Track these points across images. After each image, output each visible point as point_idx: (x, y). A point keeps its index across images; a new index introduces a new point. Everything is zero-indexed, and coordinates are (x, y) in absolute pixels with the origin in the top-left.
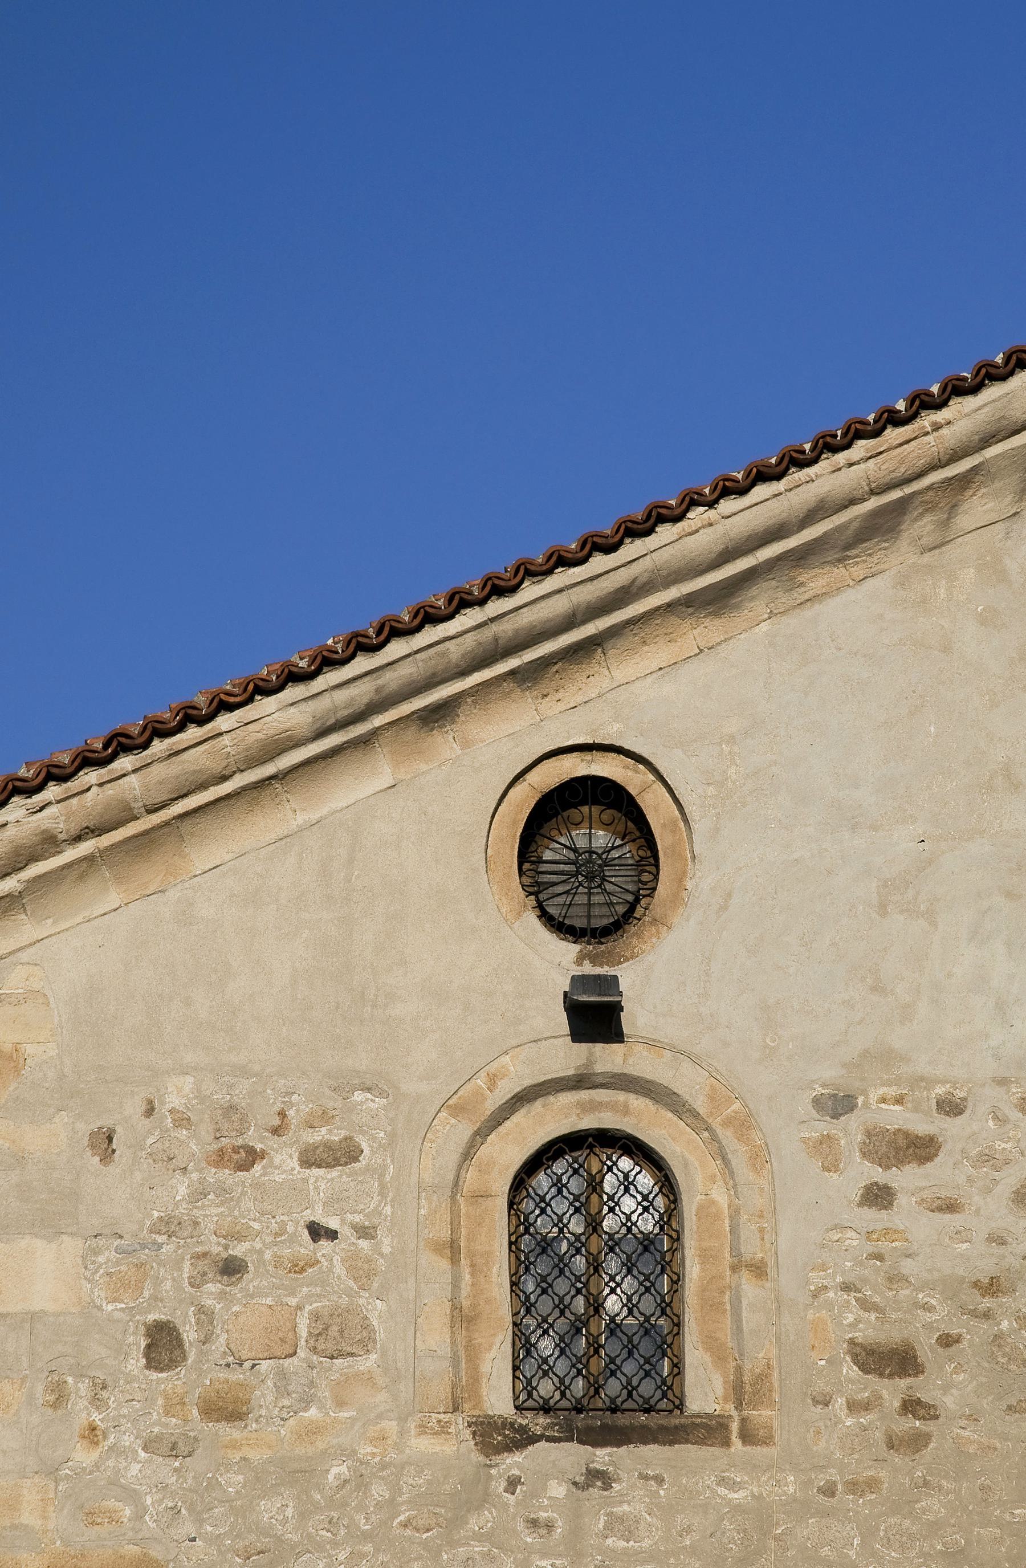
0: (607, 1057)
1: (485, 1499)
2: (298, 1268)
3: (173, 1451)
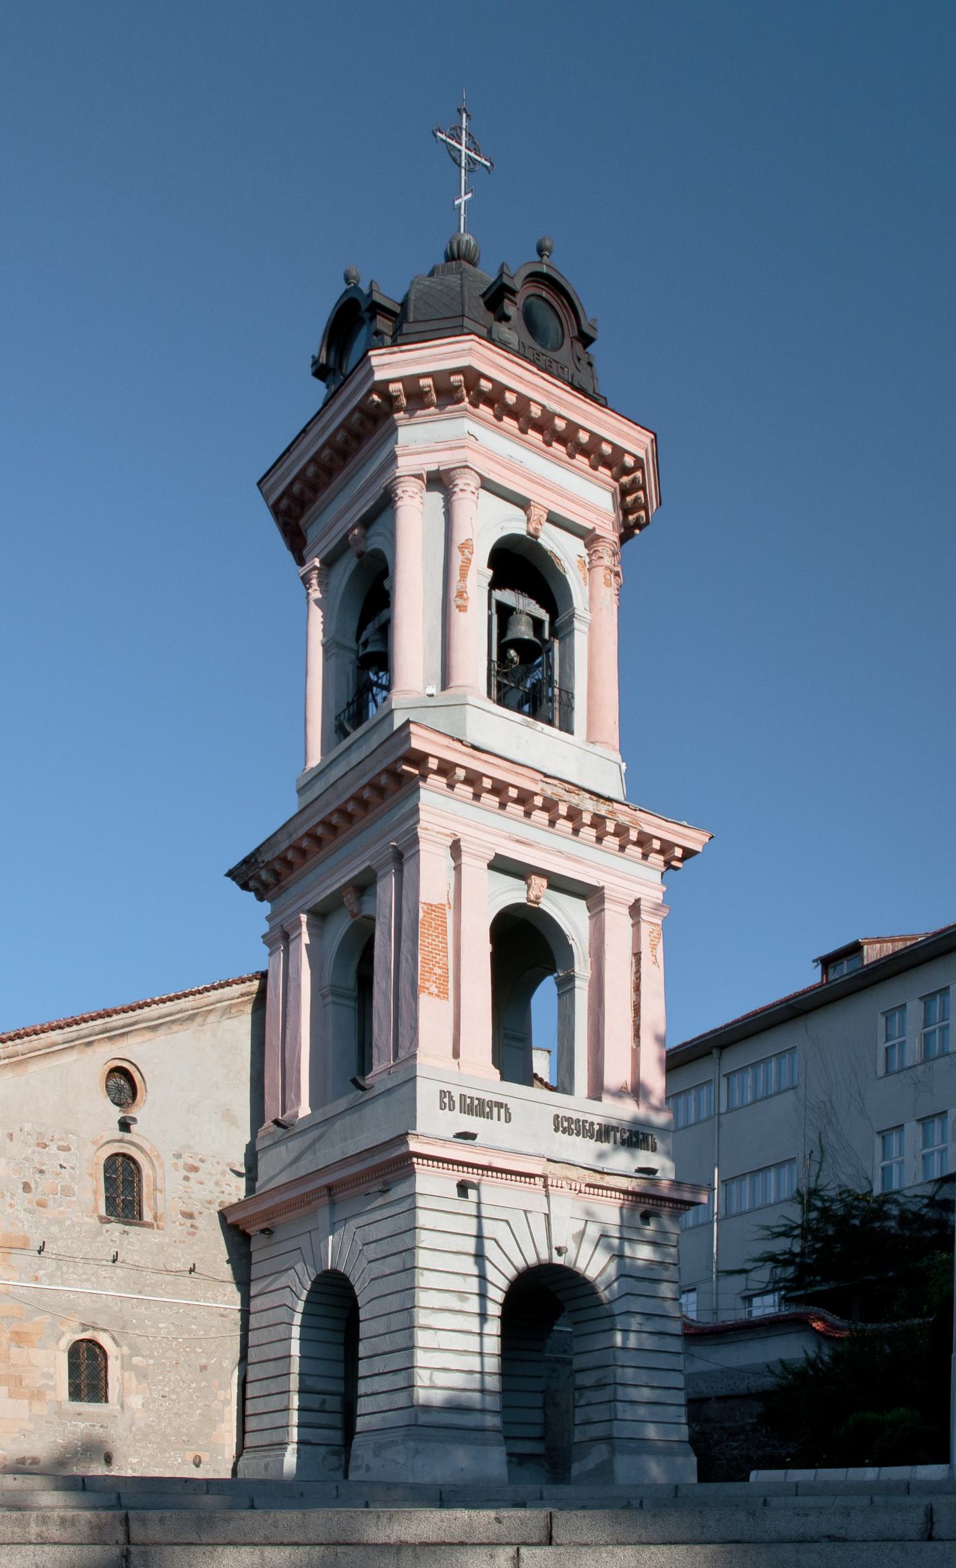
0: (127, 1136)
1: (101, 1234)
3: (30, 1212)
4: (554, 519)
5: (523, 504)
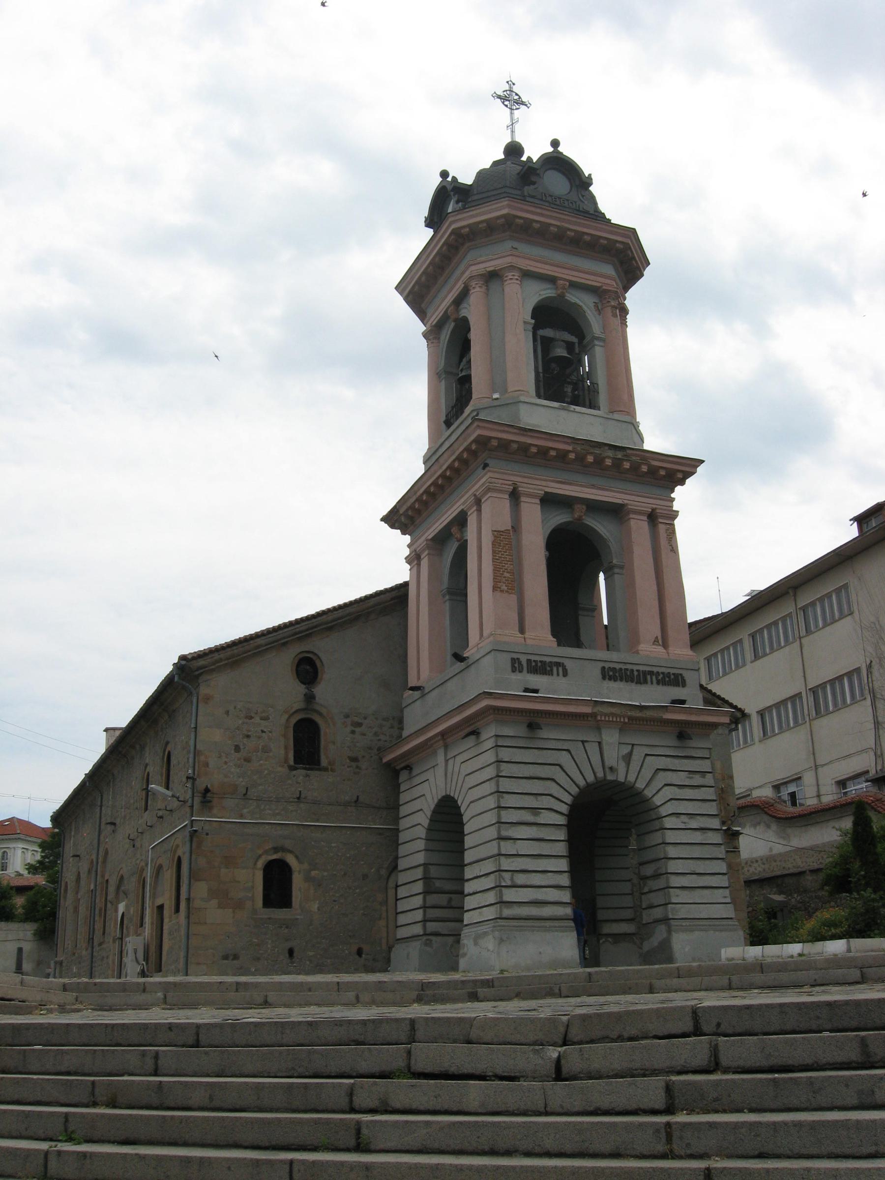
2: (259, 737)
4: (574, 285)
5: (552, 280)
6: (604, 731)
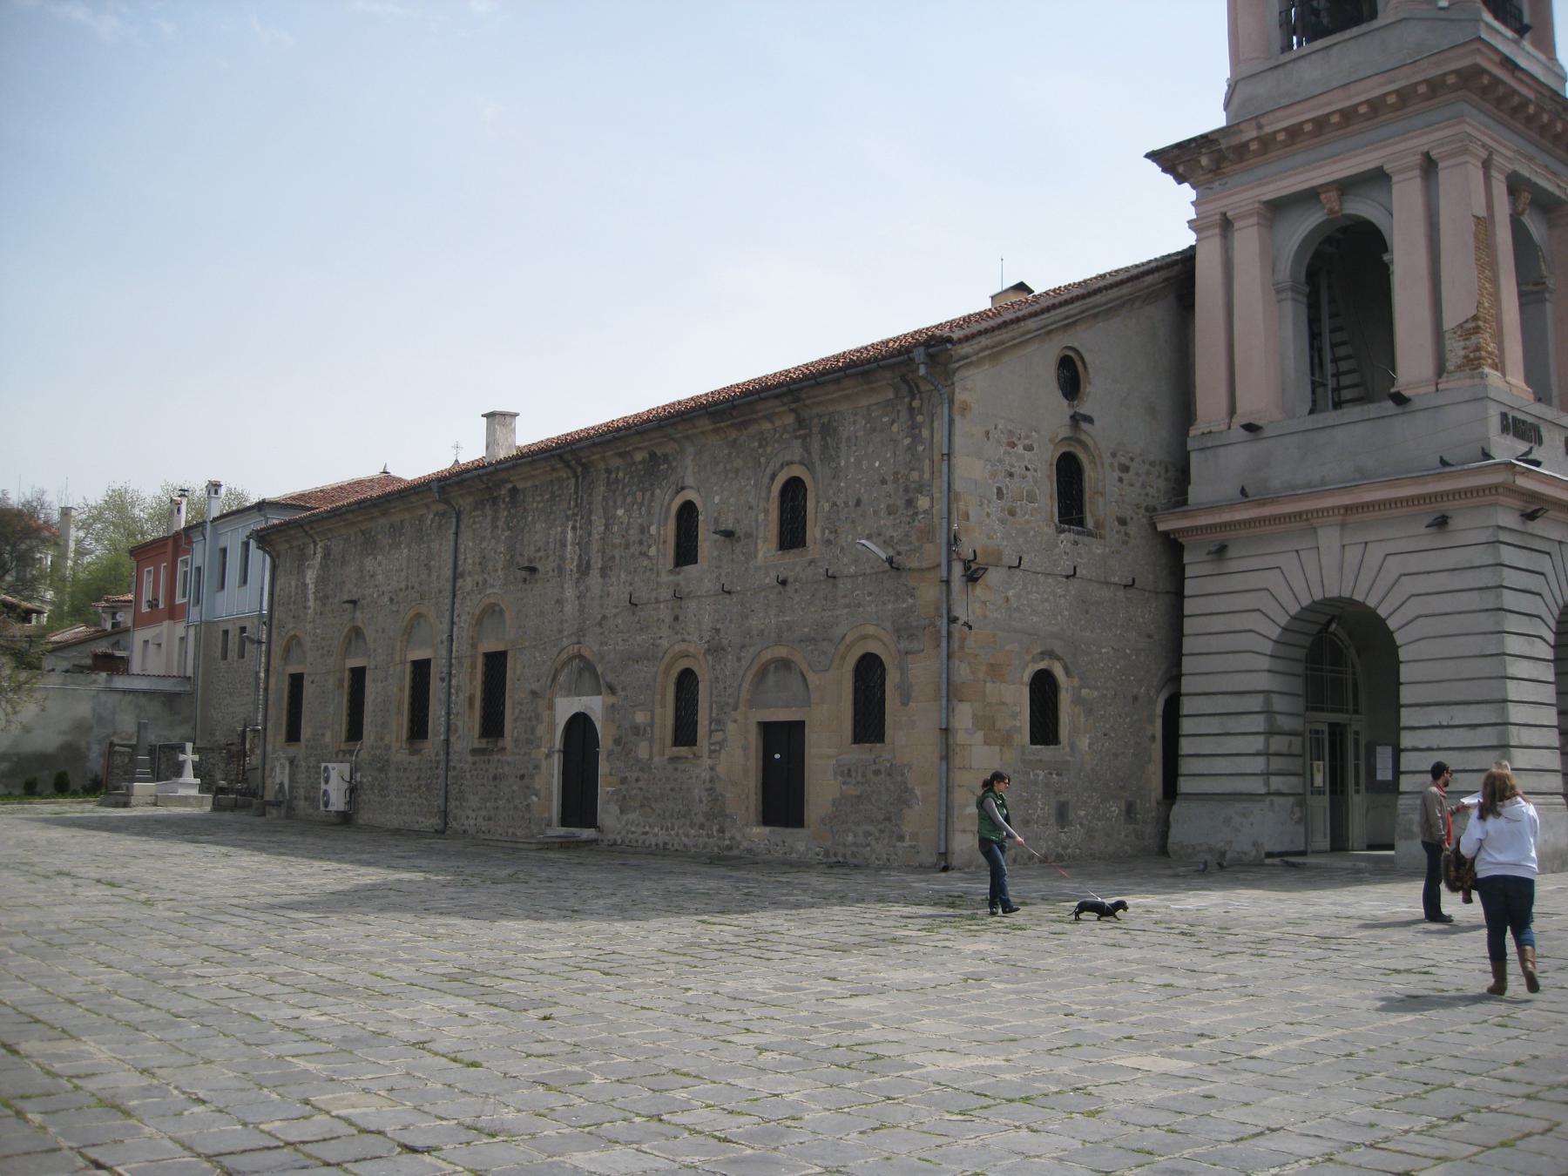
6: (1320, 532)
